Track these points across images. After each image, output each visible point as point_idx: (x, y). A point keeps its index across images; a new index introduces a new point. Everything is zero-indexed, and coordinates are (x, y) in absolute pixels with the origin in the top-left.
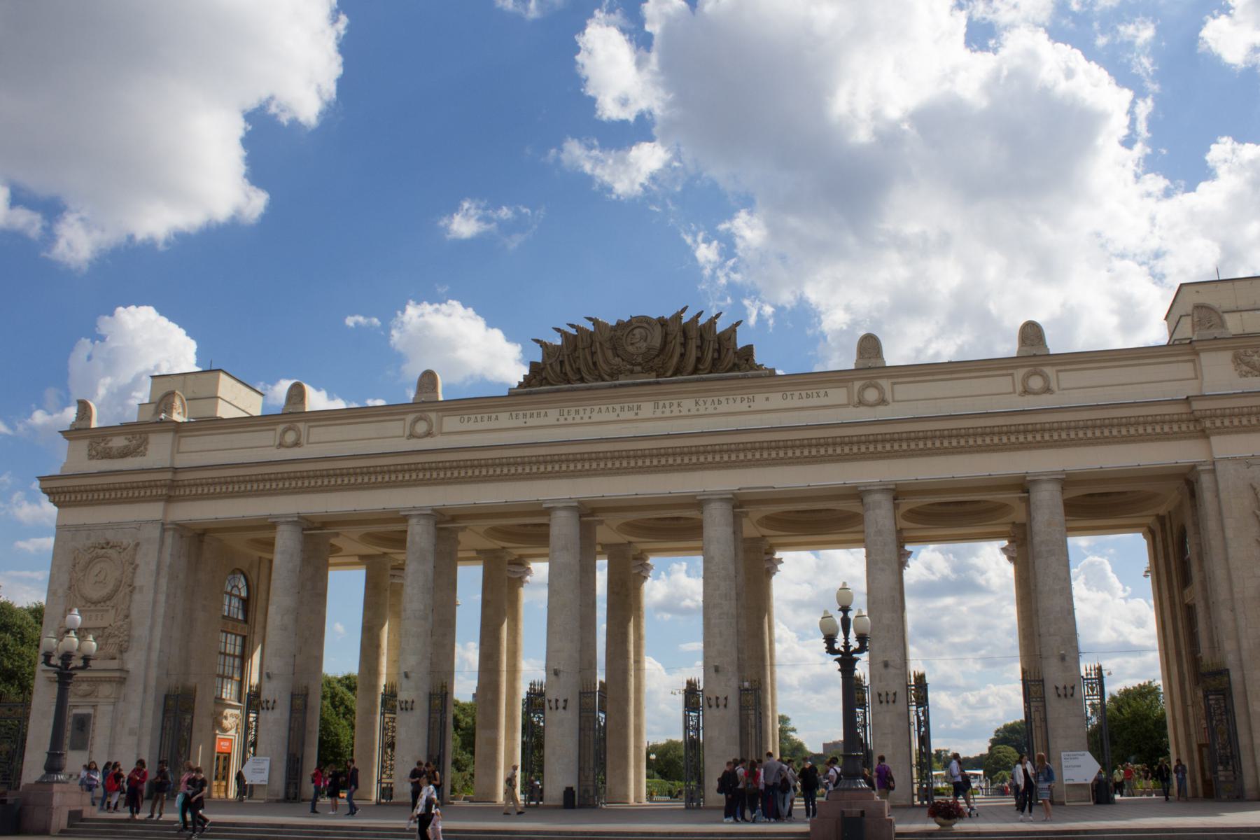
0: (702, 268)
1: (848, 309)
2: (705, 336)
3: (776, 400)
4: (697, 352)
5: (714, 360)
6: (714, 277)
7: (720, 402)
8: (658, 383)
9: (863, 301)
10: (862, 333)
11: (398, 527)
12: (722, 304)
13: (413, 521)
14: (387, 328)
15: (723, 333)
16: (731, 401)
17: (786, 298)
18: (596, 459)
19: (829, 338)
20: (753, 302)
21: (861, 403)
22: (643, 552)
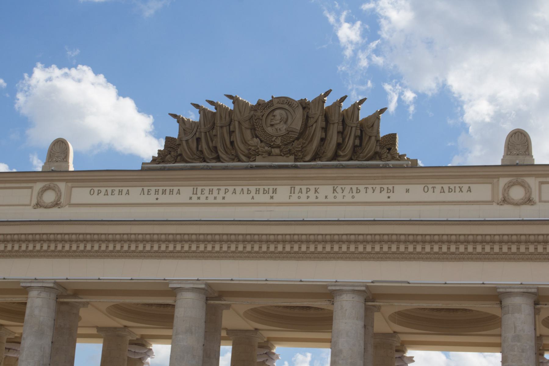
0: (344, 48)
1: (492, 100)
2: (348, 122)
3: (417, 192)
4: (340, 138)
5: (355, 146)
6: (354, 60)
7: (358, 191)
8: (296, 167)
9: (510, 93)
10: (509, 128)
11: (18, 299)
12: (362, 88)
13: (33, 294)
14: (12, 90)
15: (366, 120)
16: (370, 191)
17: (428, 84)
18: (227, 241)
19: (471, 130)
20: (394, 86)
21: (505, 201)
22: (269, 340)
